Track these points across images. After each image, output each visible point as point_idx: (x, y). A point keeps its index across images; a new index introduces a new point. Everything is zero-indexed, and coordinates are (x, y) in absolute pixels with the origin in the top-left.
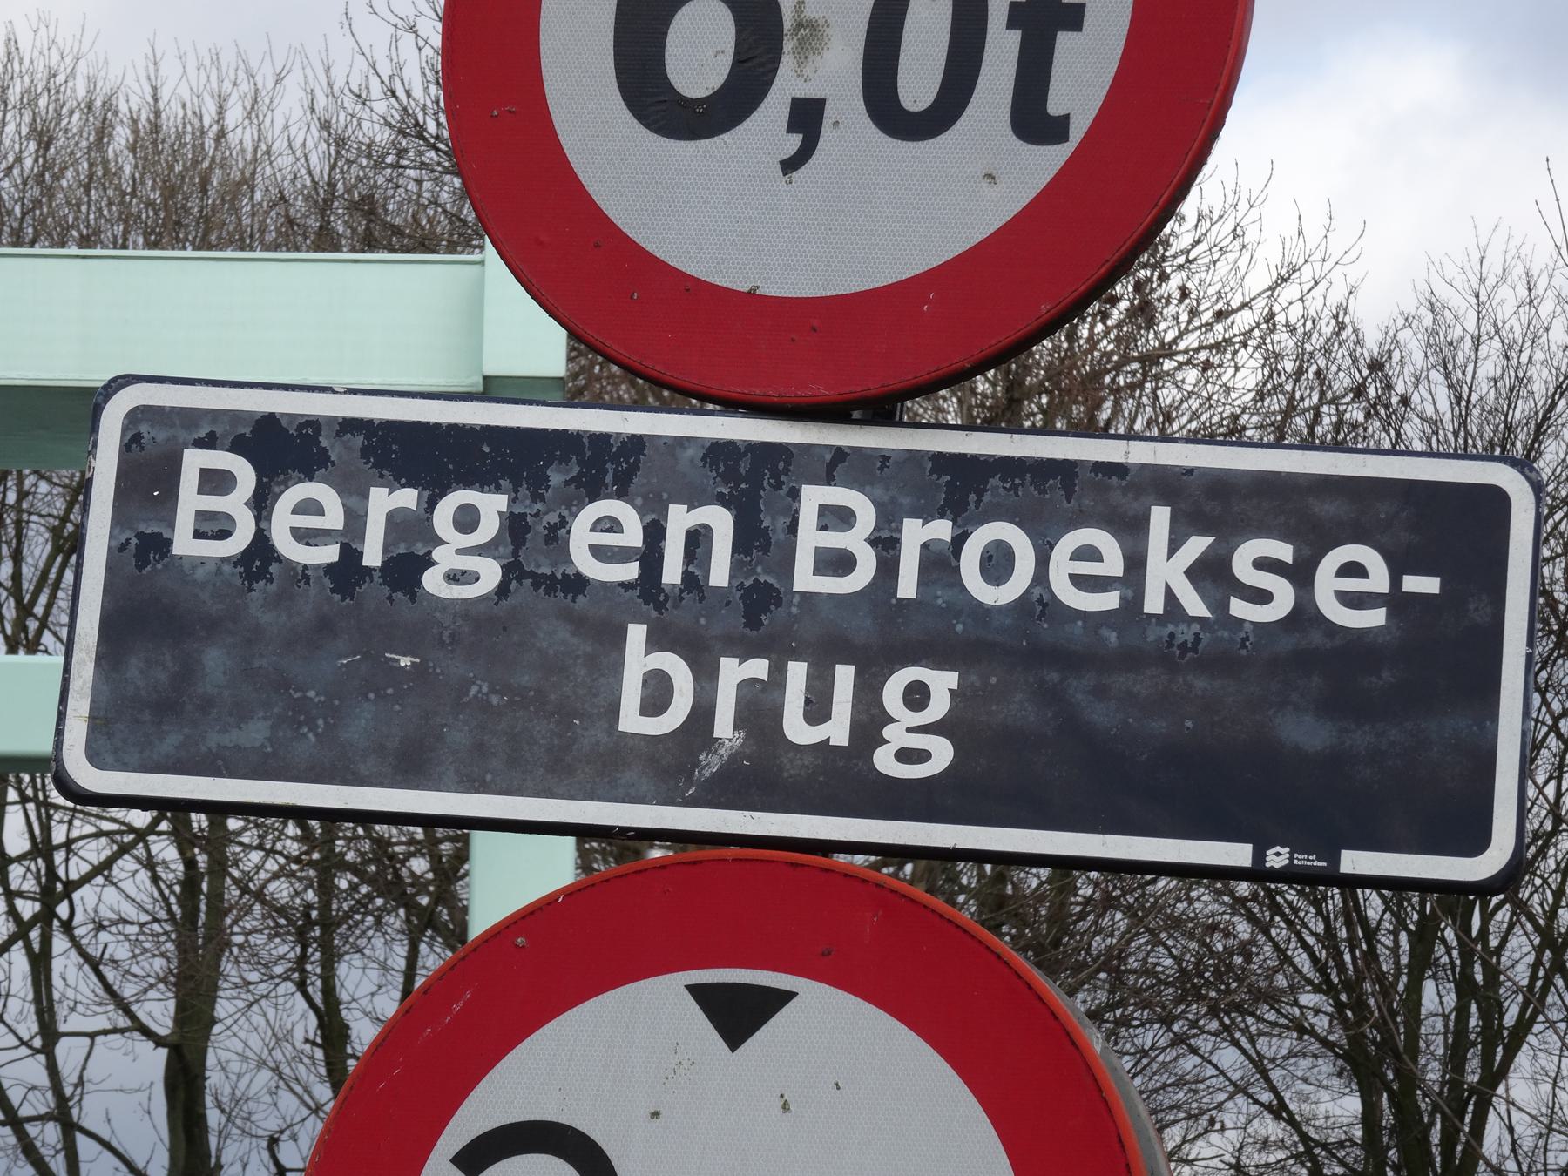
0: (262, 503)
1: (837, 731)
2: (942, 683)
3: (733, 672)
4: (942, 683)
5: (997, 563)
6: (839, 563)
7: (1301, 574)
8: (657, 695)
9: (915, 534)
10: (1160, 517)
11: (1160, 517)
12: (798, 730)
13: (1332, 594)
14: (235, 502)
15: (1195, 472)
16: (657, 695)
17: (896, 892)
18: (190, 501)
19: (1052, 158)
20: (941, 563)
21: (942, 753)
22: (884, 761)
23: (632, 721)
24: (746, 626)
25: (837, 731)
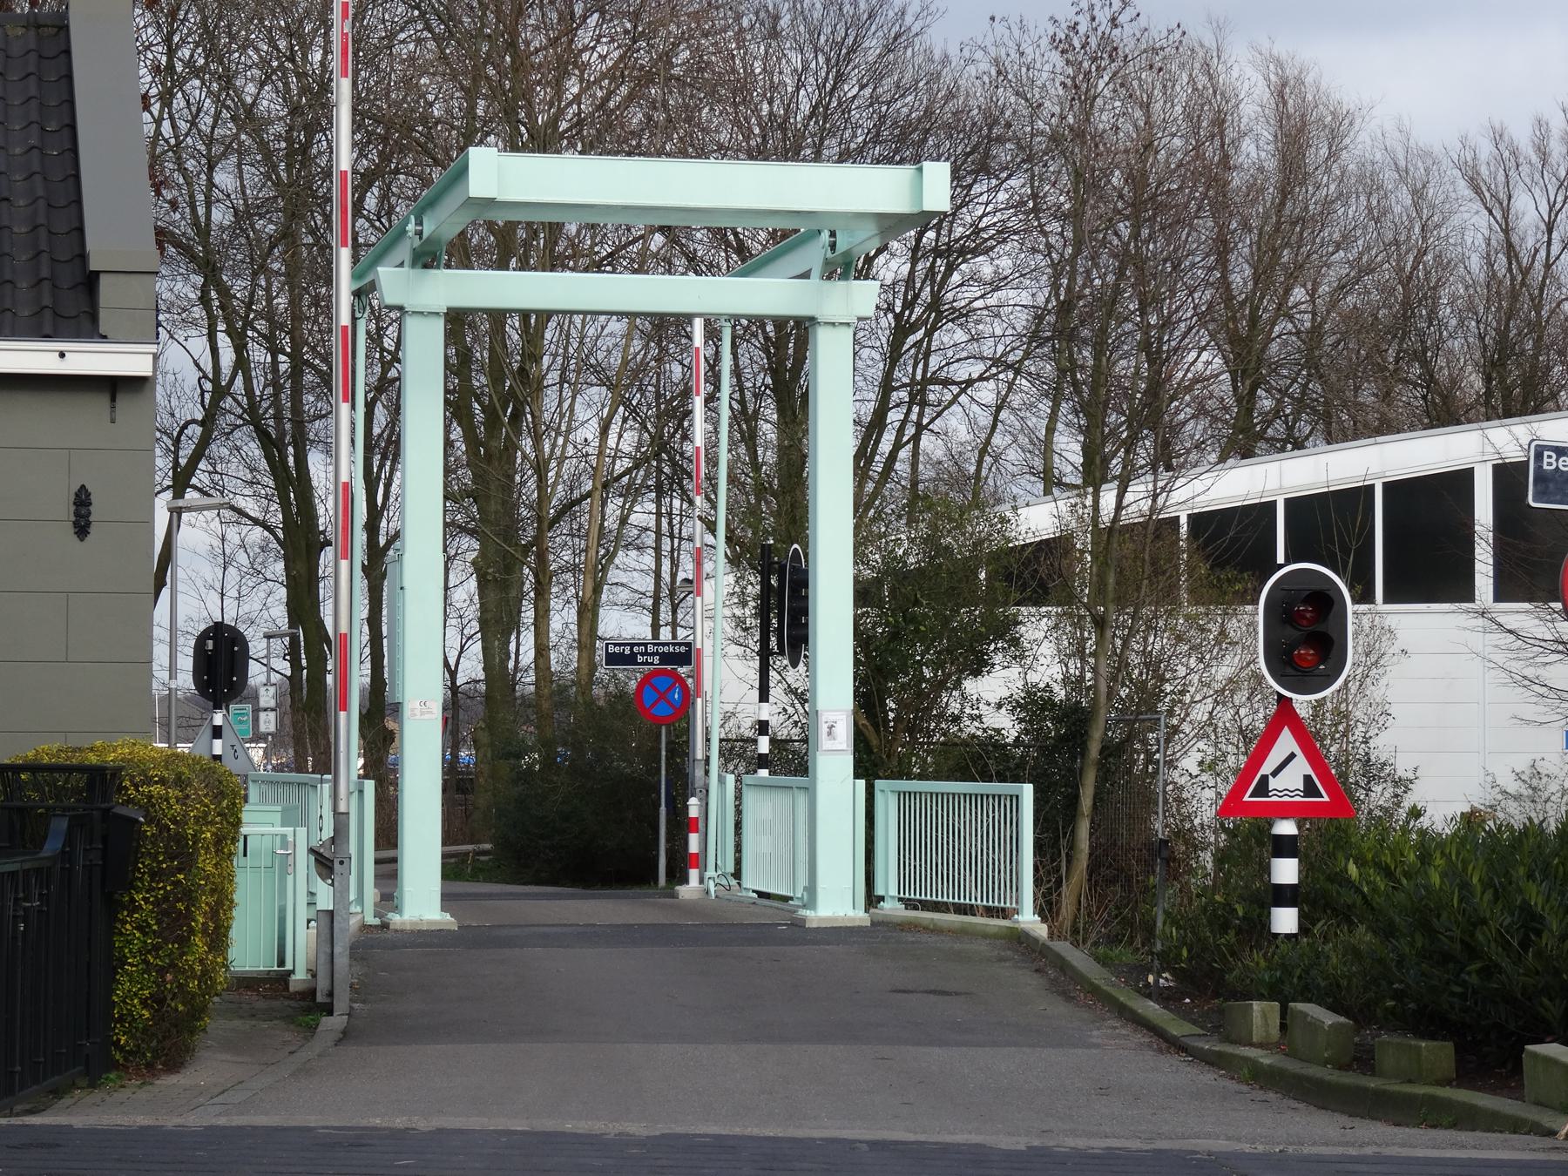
0: (1557, 460)
6: (1550, 464)
14: (1553, 460)
18: (1546, 460)
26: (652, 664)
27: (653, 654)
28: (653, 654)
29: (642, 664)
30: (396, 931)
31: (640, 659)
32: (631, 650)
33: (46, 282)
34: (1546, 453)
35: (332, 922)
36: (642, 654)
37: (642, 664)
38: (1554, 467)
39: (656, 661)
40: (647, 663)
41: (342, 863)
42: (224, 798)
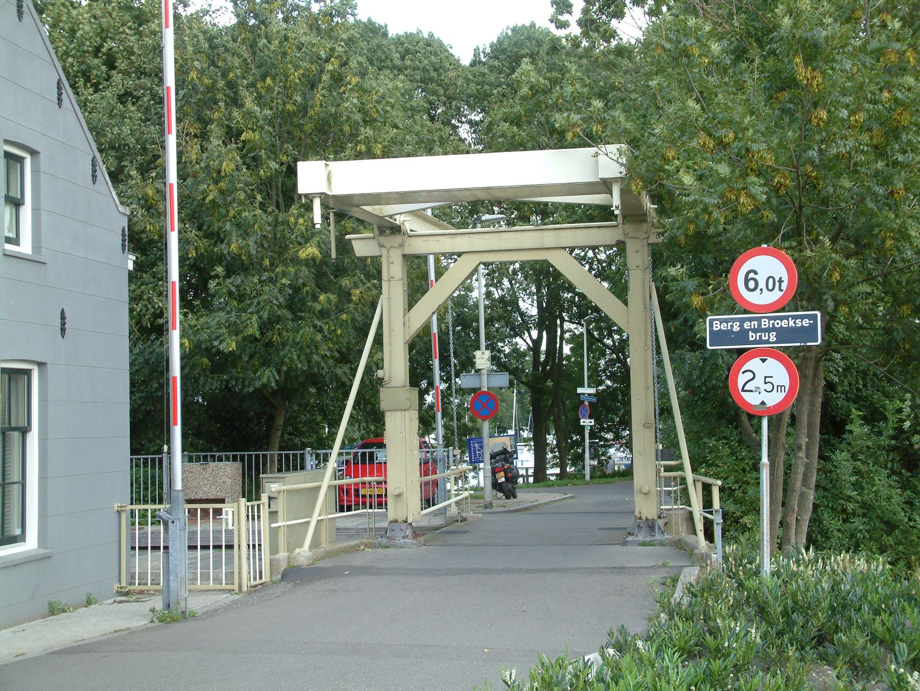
1: (767, 338)
2: (775, 333)
3: (758, 334)
4: (775, 333)
5: (778, 324)
6: (765, 325)
7: (802, 322)
8: (752, 337)
9: (771, 322)
10: (790, 319)
11: (790, 319)
12: (763, 338)
13: (2, 155)
14: (718, 325)
15: (177, 57)
16: (752, 337)
17: (215, 610)
18: (715, 326)
19: (782, 293)
20: (773, 324)
21: (775, 339)
22: (771, 340)
23: (751, 339)
24: (479, 349)
25: (767, 338)
26: (767, 342)
27: (769, 330)
28: (769, 330)
29: (755, 342)
30: (235, 459)
31: (752, 336)
32: (741, 326)
33: (16, 486)
34: (715, 322)
35: (21, 564)
36: (755, 331)
37: (755, 342)
38: (767, 326)
39: (773, 338)
40: (761, 341)
41: (173, 522)
42: (515, 303)
